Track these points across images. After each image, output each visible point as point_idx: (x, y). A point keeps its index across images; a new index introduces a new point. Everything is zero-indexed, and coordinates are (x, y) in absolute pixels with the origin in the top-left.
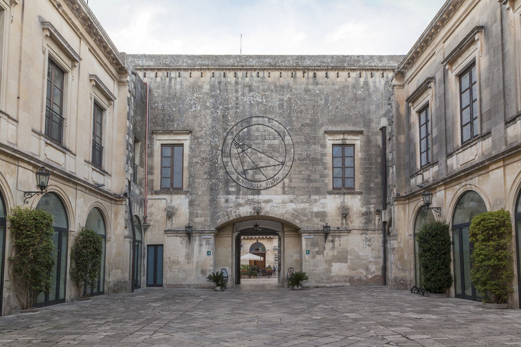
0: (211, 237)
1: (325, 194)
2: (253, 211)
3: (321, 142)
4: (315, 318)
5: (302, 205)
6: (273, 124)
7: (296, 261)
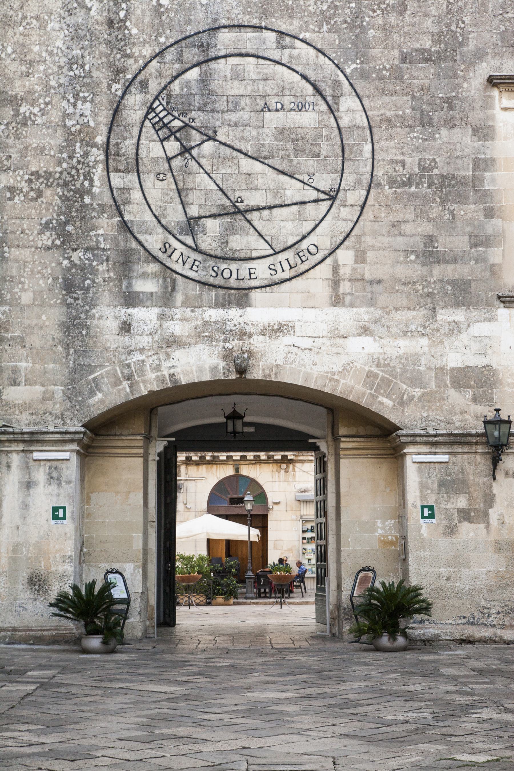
0: (66, 455)
1: (489, 305)
2: (222, 364)
3: (476, 116)
4: (466, 757)
5: (405, 346)
6: (295, 52)
7: (386, 543)
